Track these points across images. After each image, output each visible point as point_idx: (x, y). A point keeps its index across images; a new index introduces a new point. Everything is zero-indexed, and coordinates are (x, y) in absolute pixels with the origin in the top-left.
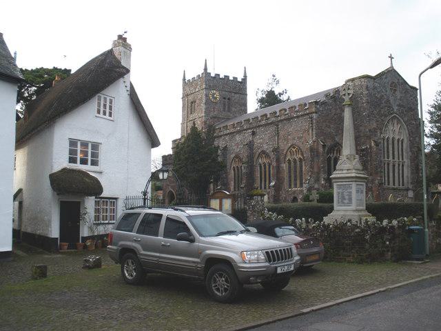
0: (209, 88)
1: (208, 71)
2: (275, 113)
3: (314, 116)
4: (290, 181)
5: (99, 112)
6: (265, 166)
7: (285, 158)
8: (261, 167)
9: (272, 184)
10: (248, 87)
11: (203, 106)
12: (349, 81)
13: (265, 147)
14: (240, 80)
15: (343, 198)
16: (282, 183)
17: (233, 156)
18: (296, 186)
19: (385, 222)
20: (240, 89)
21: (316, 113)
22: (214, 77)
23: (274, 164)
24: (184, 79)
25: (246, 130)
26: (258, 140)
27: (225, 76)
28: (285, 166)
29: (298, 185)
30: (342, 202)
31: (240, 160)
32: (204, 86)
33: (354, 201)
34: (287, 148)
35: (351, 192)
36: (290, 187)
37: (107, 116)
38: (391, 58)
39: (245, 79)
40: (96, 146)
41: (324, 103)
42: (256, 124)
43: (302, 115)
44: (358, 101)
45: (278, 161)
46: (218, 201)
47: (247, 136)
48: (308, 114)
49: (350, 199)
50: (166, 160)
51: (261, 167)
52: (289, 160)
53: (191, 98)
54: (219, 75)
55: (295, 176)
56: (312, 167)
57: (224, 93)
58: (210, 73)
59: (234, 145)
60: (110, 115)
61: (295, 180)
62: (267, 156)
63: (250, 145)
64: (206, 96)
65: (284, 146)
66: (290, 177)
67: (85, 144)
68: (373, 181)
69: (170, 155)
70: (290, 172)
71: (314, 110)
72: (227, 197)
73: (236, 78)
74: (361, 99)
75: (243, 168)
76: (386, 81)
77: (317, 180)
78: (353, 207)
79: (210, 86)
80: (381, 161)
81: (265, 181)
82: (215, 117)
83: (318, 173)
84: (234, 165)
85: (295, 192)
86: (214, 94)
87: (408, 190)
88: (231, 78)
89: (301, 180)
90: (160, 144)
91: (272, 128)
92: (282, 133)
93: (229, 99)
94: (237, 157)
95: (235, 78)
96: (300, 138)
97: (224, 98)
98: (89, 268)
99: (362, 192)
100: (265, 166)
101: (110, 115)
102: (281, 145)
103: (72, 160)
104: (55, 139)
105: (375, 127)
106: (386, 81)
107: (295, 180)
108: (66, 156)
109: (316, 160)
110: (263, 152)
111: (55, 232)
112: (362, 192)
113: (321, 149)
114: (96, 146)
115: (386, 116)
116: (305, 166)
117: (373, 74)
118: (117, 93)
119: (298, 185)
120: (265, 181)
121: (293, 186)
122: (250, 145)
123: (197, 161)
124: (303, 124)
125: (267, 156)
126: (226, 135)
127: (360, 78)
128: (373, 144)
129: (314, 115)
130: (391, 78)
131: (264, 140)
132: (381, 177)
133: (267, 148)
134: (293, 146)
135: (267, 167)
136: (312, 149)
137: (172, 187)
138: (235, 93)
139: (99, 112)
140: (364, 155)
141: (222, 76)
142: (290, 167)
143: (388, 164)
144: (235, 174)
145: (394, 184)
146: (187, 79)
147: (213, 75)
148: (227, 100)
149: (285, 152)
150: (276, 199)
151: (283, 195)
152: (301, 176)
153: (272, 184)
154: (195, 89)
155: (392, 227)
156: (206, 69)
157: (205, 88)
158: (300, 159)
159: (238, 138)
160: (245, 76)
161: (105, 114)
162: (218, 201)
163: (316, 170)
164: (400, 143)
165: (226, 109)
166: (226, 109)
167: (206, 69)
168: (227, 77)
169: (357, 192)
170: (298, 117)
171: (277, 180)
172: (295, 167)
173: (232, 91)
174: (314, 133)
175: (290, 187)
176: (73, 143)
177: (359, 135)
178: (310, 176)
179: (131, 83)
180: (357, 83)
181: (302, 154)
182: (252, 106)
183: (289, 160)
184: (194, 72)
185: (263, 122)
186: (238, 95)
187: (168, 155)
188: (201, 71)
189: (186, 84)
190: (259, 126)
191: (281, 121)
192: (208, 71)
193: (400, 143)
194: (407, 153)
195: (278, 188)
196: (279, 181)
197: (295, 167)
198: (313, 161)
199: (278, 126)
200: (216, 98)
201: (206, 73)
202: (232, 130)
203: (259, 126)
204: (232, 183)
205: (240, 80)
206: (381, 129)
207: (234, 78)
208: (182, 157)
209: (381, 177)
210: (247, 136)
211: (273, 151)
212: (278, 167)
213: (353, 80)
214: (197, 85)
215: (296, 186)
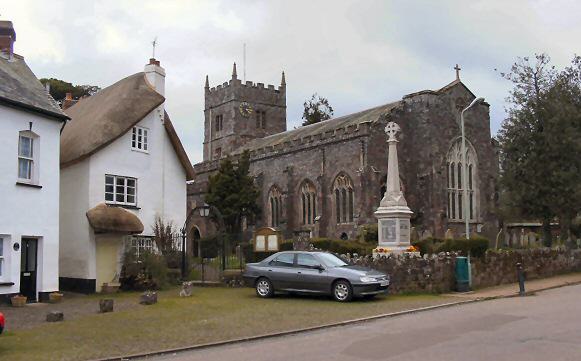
0: (239, 99)
2: (321, 134)
4: (338, 214)
5: (134, 146)
6: (309, 197)
8: (304, 199)
9: (318, 218)
11: (232, 123)
12: (407, 97)
13: (309, 175)
15: (388, 234)
16: (330, 216)
17: (270, 185)
19: (426, 256)
20: (277, 100)
21: (368, 135)
23: (320, 194)
24: (207, 87)
28: (332, 197)
29: (348, 219)
30: (386, 238)
31: (279, 190)
33: (398, 237)
35: (395, 228)
37: (142, 149)
38: (457, 69)
40: (131, 182)
42: (298, 146)
46: (263, 237)
49: (394, 235)
51: (304, 199)
52: (337, 190)
53: (216, 111)
55: (344, 204)
56: (363, 198)
59: (270, 174)
60: (145, 148)
61: (344, 213)
62: (312, 185)
66: (338, 209)
67: (121, 181)
70: (338, 204)
71: (365, 132)
72: (273, 233)
76: (452, 96)
78: (397, 242)
79: (240, 97)
80: (444, 191)
81: (309, 215)
82: (245, 136)
84: (271, 195)
86: (246, 107)
88: (266, 87)
89: (351, 213)
91: (315, 155)
92: (328, 158)
94: (275, 186)
96: (349, 165)
98: (147, 303)
99: (406, 228)
100: (309, 197)
101: (145, 148)
103: (109, 197)
104: (91, 180)
105: (437, 151)
106: (452, 96)
107: (344, 213)
108: (103, 192)
110: (307, 181)
112: (406, 228)
113: (373, 179)
114: (131, 182)
115: (450, 138)
117: (436, 88)
118: (154, 128)
119: (348, 219)
120: (309, 215)
125: (312, 185)
126: (263, 159)
127: (421, 93)
128: (434, 172)
130: (458, 93)
131: (306, 167)
132: (445, 209)
134: (342, 174)
135: (311, 198)
136: (362, 179)
139: (134, 146)
140: (414, 189)
142: (338, 198)
143: (453, 194)
145: (460, 218)
146: (211, 86)
148: (261, 114)
150: (322, 233)
151: (330, 230)
152: (351, 208)
153: (318, 218)
155: (433, 261)
156: (235, 76)
158: (350, 189)
159: (277, 162)
161: (140, 147)
162: (263, 237)
163: (368, 201)
167: (235, 76)
169: (401, 227)
172: (344, 198)
173: (264, 104)
176: (109, 179)
179: (165, 113)
181: (353, 185)
182: (294, 121)
183: (337, 190)
184: (220, 77)
185: (307, 145)
189: (209, 92)
194: (477, 181)
195: (324, 224)
196: (326, 213)
197: (344, 198)
198: (363, 191)
202: (269, 154)
204: (270, 218)
206: (444, 154)
209: (445, 209)
212: (324, 200)
213: (411, 96)
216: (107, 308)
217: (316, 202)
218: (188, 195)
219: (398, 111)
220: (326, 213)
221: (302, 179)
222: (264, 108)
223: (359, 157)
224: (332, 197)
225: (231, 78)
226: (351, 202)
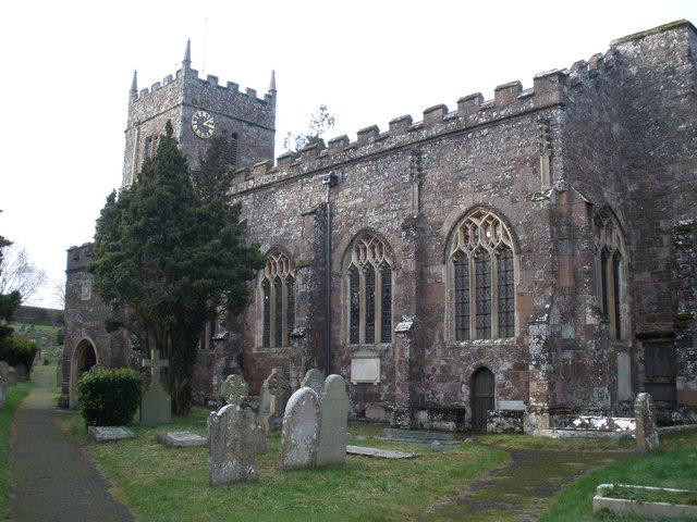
0: (191, 104)
1: (193, 66)
3: (558, 115)
7: (446, 248)
10: (277, 114)
13: (373, 218)
18: (484, 331)
20: (261, 117)
22: (206, 83)
23: (410, 265)
24: (134, 90)
26: (346, 201)
27: (231, 84)
28: (444, 273)
29: (494, 330)
32: (181, 99)
34: (454, 215)
36: (462, 332)
39: (272, 96)
41: (576, 85)
43: (508, 118)
44: (657, 92)
45: (421, 256)
47: (314, 193)
50: (77, 259)
52: (460, 254)
54: (216, 79)
57: (224, 119)
58: (196, 72)
63: (323, 214)
64: (185, 121)
65: (445, 215)
68: (283, 365)
69: (89, 245)
71: (554, 98)
73: (254, 92)
74: (670, 86)
75: (299, 280)
77: (570, 314)
81: (370, 321)
83: (575, 291)
85: (481, 352)
86: (203, 119)
88: (242, 90)
90: (70, 251)
91: (400, 166)
92: (433, 176)
93: (235, 136)
95: (252, 92)
97: (224, 131)
102: (432, 210)
109: (565, 246)
110: (367, 234)
116: (524, 268)
121: (472, 332)
122: (323, 214)
123: (174, 241)
127: (663, 29)
133: (387, 222)
136: (554, 217)
137: (90, 331)
138: (250, 124)
141: (223, 83)
144: (267, 305)
146: (140, 88)
147: (203, 76)
149: (446, 229)
151: (437, 360)
153: (406, 325)
154: (159, 108)
156: (187, 61)
157: (183, 104)
159: (282, 200)
160: (274, 91)
163: (566, 281)
164: (610, 260)
167: (187, 61)
168: (233, 86)
170: (493, 123)
171: (417, 313)
174: (559, 165)
175: (462, 332)
177: (667, 188)
178: (552, 300)
180: (653, 44)
183: (460, 254)
184: (160, 68)
186: (255, 130)
187: (83, 247)
188: (173, 66)
190: (353, 162)
191: (430, 139)
192: (193, 66)
193: (610, 260)
196: (426, 316)
199: (419, 154)
200: (205, 129)
201: (190, 73)
203: (353, 162)
204: (260, 325)
205: (261, 96)
207: (249, 90)
208: (125, 228)
210: (314, 193)
211: (405, 228)
213: (637, 38)
214: (162, 97)
215: (484, 331)
216: (289, 134)
217: (395, 289)
218: (69, 272)
219: (607, 68)
220: (426, 316)
221: (354, 231)
222: (46, 367)
223: (535, 162)
224: (444, 273)
225: (180, 66)
226: (386, 290)
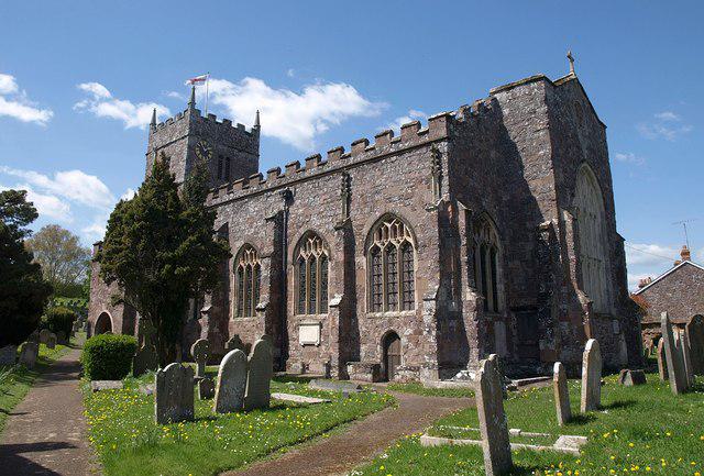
14: (248, 128)
25: (272, 190)
34: (371, 220)
43: (410, 149)
48: (427, 144)
54: (214, 117)
85: (390, 321)
87: (612, 318)
88: (234, 125)
95: (241, 127)
110: (312, 234)
111: (259, 306)
116: (421, 259)
124: (422, 164)
129: (444, 144)
155: (42, 314)
160: (258, 126)
165: (223, 176)
166: (223, 176)
167: (193, 103)
185: (314, 171)
190: (303, 181)
201: (195, 112)
203: (303, 181)
